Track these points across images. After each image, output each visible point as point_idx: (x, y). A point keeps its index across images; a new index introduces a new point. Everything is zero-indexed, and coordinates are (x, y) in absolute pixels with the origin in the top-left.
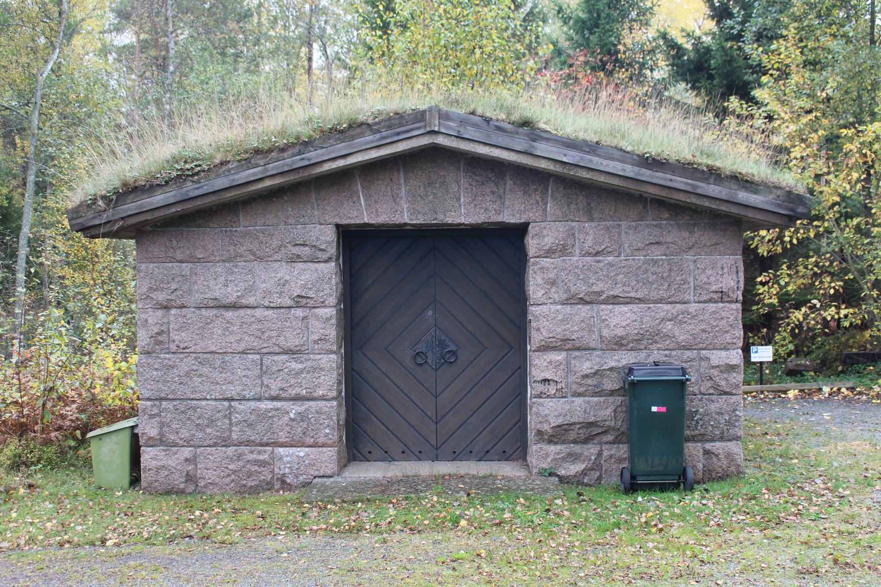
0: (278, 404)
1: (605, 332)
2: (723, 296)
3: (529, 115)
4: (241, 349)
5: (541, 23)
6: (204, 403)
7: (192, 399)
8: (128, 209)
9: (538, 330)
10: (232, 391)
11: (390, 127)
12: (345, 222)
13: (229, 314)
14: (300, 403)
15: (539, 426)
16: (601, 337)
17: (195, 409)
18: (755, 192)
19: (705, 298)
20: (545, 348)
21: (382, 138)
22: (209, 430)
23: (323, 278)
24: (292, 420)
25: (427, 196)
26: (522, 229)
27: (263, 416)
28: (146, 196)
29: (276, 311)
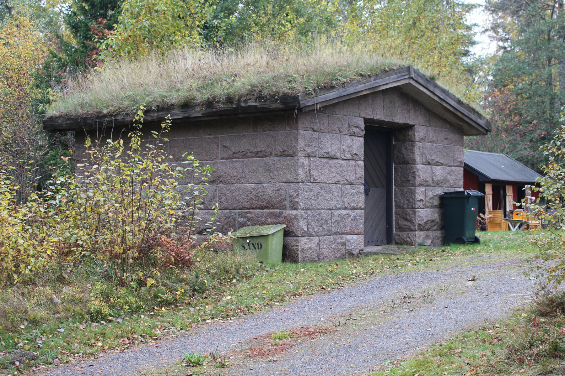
0: (347, 211)
1: (434, 178)
2: (354, 157)
3: (254, 80)
4: (335, 181)
5: (63, 60)
6: (322, 211)
7: (319, 209)
8: (321, 99)
9: (419, 176)
10: (332, 204)
11: (400, 73)
12: (367, 117)
13: (331, 162)
14: (353, 211)
15: (420, 222)
16: (433, 180)
17: (319, 214)
18: (481, 119)
19: (456, 164)
20: (421, 185)
21: (398, 77)
22: (324, 227)
23: (357, 144)
24: (352, 220)
25: (390, 108)
26: (409, 127)
27: (342, 218)
28: (327, 92)
29: (345, 161)
